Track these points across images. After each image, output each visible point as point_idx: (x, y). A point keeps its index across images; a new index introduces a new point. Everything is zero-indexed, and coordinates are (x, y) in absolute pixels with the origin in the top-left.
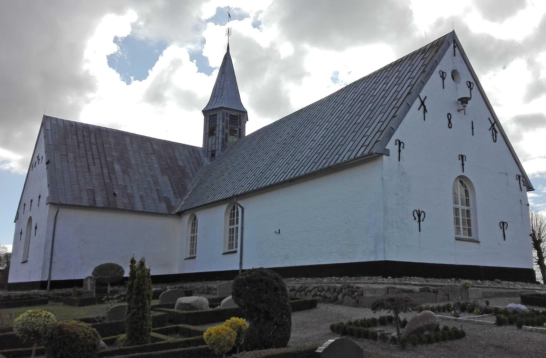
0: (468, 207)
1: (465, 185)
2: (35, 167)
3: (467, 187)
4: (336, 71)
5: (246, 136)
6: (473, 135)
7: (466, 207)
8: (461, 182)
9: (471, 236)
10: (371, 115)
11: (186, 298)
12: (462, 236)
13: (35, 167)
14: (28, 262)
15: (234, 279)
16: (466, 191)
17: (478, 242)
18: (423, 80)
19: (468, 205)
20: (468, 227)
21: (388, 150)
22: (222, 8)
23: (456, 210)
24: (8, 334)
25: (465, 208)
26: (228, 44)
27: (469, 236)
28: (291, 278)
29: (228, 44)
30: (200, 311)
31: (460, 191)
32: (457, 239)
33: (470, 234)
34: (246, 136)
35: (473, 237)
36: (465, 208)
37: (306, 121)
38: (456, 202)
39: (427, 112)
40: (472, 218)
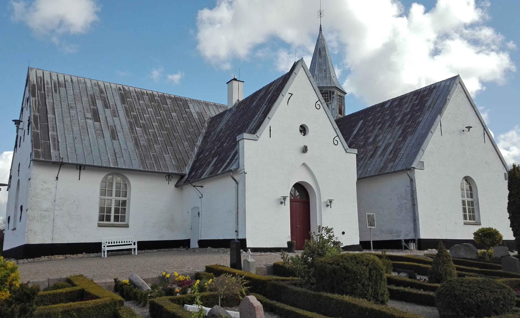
2: (20, 147)
4: (478, 53)
5: (3, 250)
6: (79, 180)
7: (470, 199)
8: (465, 180)
13: (20, 147)
14: (16, 230)
16: (470, 187)
19: (472, 197)
23: (464, 202)
25: (470, 199)
26: (321, 25)
29: (321, 25)
31: (466, 186)
32: (465, 224)
34: (3, 250)
36: (470, 199)
38: (463, 196)
40: (475, 207)
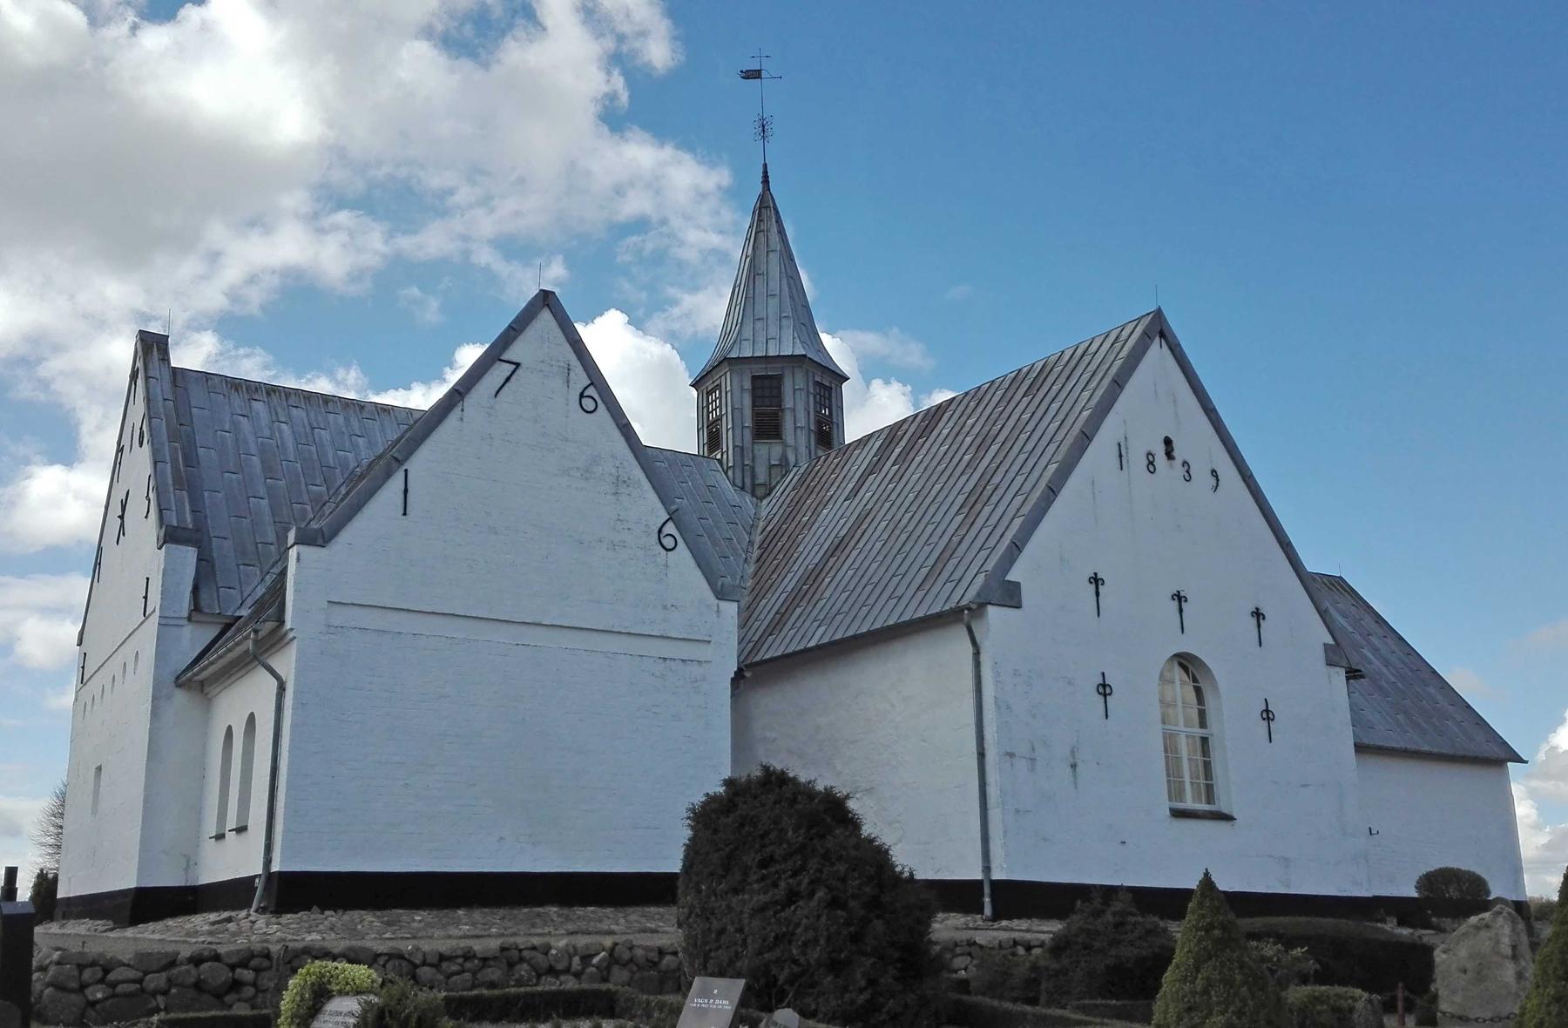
0: (1202, 731)
1: (1193, 674)
3: (1200, 681)
9: (1214, 804)
10: (1026, 502)
11: (593, 912)
12: (1189, 803)
15: (1064, 919)
17: (1228, 818)
18: (1084, 430)
19: (1203, 724)
20: (1207, 780)
21: (1016, 586)
22: (214, 331)
24: (482, 995)
27: (1209, 803)
28: (1162, 918)
30: (974, 998)
32: (1178, 814)
33: (1210, 798)
35: (1222, 805)
37: (840, 518)
39: (122, 501)
